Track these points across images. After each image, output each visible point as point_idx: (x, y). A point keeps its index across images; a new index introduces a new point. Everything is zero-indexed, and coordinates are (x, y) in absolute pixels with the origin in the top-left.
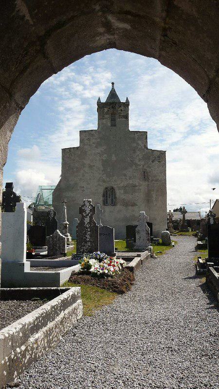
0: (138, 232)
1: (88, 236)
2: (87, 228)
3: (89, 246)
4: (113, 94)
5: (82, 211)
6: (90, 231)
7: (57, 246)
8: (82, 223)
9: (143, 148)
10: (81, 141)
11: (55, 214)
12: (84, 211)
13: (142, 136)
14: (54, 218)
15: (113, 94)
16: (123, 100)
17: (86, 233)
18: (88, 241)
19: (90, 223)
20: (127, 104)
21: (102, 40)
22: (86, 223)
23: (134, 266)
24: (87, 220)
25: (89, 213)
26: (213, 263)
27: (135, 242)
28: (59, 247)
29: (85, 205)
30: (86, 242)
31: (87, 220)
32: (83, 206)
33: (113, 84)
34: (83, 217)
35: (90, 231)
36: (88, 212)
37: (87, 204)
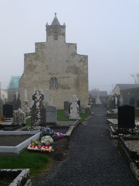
0: (72, 108)
1: (39, 115)
2: (38, 109)
3: (40, 122)
4: (56, 20)
5: (34, 98)
6: (40, 112)
7: (19, 119)
8: (35, 106)
9: (74, 53)
10: (36, 49)
11: (19, 96)
12: (36, 98)
13: (75, 46)
14: (18, 99)
15: (56, 20)
16: (62, 24)
17: (37, 113)
18: (39, 118)
19: (39, 106)
20: (64, 27)
21: (24, 76)
22: (37, 106)
23: (120, 89)
24: (38, 104)
25: (39, 99)
26: (111, 127)
27: (70, 113)
28: (21, 119)
29: (36, 94)
30: (37, 119)
31: (38, 104)
32: (35, 95)
33: (56, 14)
34: (35, 102)
35: (40, 112)
36: (38, 99)
37: (38, 93)
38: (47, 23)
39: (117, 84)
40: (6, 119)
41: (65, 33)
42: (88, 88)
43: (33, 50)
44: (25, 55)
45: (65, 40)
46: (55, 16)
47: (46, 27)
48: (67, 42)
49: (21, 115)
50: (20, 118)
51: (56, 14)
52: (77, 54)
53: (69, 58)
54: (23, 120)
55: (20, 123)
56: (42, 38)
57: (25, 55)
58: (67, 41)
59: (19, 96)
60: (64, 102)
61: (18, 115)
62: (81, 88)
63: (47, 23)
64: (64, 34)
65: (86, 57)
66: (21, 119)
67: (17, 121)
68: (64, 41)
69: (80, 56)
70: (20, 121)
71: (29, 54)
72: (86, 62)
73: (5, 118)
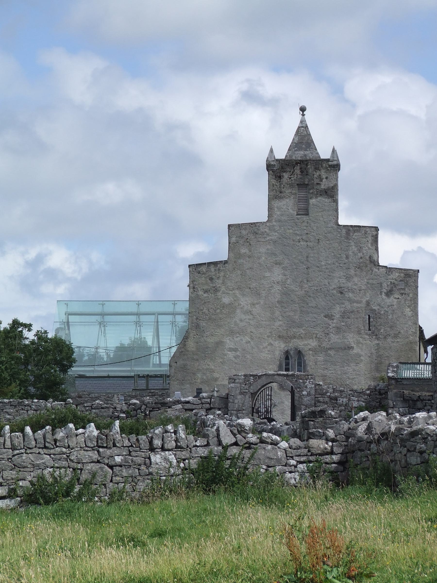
33: (303, 109)
38: (271, 151)
51: (303, 109)
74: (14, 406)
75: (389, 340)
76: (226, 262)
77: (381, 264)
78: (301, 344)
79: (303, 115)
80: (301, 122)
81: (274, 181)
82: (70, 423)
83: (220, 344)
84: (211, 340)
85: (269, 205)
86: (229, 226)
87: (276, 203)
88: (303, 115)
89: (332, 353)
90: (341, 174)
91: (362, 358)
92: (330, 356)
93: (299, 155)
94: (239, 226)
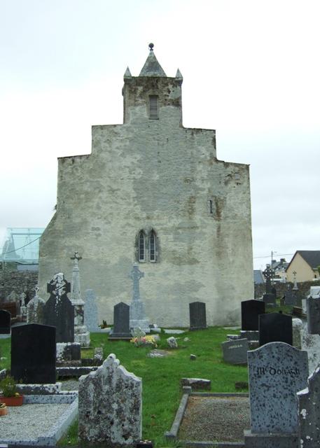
4: (152, 64)
7: (110, 410)
15: (152, 64)
16: (170, 73)
20: (177, 82)
28: (120, 411)
33: (151, 46)
38: (128, 69)
39: (297, 252)
40: (28, 391)
41: (180, 98)
42: (252, 262)
43: (85, 148)
44: (62, 160)
45: (181, 120)
46: (149, 52)
47: (125, 80)
48: (186, 124)
49: (119, 387)
50: (115, 406)
51: (151, 46)
52: (217, 161)
53: (92, 220)
54: (127, 414)
55: (114, 428)
56: (112, 111)
57: (62, 160)
58: (187, 123)
59: (67, 287)
60: (190, 304)
61: (106, 388)
62: (231, 260)
63: (128, 69)
64: (177, 103)
65: (241, 171)
66: (120, 411)
67: (97, 421)
68: (178, 122)
69: (227, 165)
70: (116, 421)
71: (73, 158)
72: (245, 184)
73: (21, 386)
74: (267, 386)
75: (229, 220)
76: (87, 157)
77: (219, 159)
78: (155, 224)
79: (152, 50)
80: (151, 54)
81: (61, 167)
82: (309, 389)
83: (85, 222)
84: (78, 220)
85: (67, 179)
86: (93, 127)
87: (129, 110)
88: (152, 50)
89: (180, 231)
90: (183, 85)
91: (206, 236)
92: (178, 233)
93: (150, 74)
94: (102, 127)
